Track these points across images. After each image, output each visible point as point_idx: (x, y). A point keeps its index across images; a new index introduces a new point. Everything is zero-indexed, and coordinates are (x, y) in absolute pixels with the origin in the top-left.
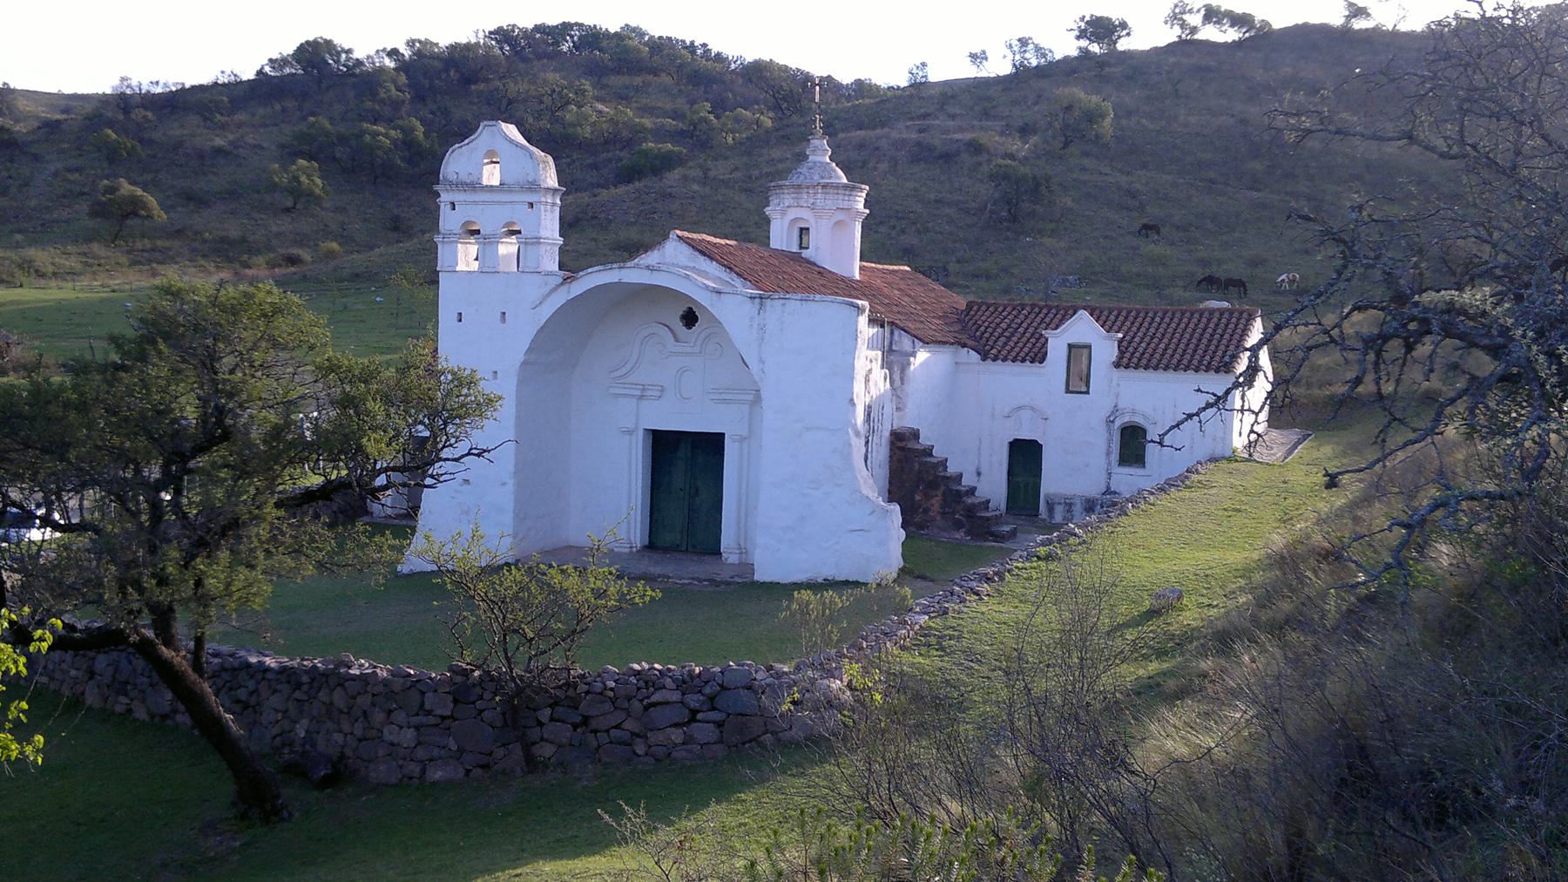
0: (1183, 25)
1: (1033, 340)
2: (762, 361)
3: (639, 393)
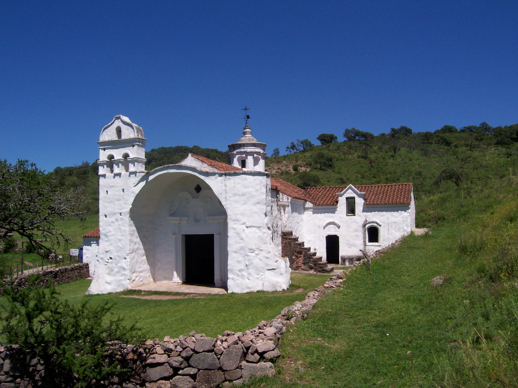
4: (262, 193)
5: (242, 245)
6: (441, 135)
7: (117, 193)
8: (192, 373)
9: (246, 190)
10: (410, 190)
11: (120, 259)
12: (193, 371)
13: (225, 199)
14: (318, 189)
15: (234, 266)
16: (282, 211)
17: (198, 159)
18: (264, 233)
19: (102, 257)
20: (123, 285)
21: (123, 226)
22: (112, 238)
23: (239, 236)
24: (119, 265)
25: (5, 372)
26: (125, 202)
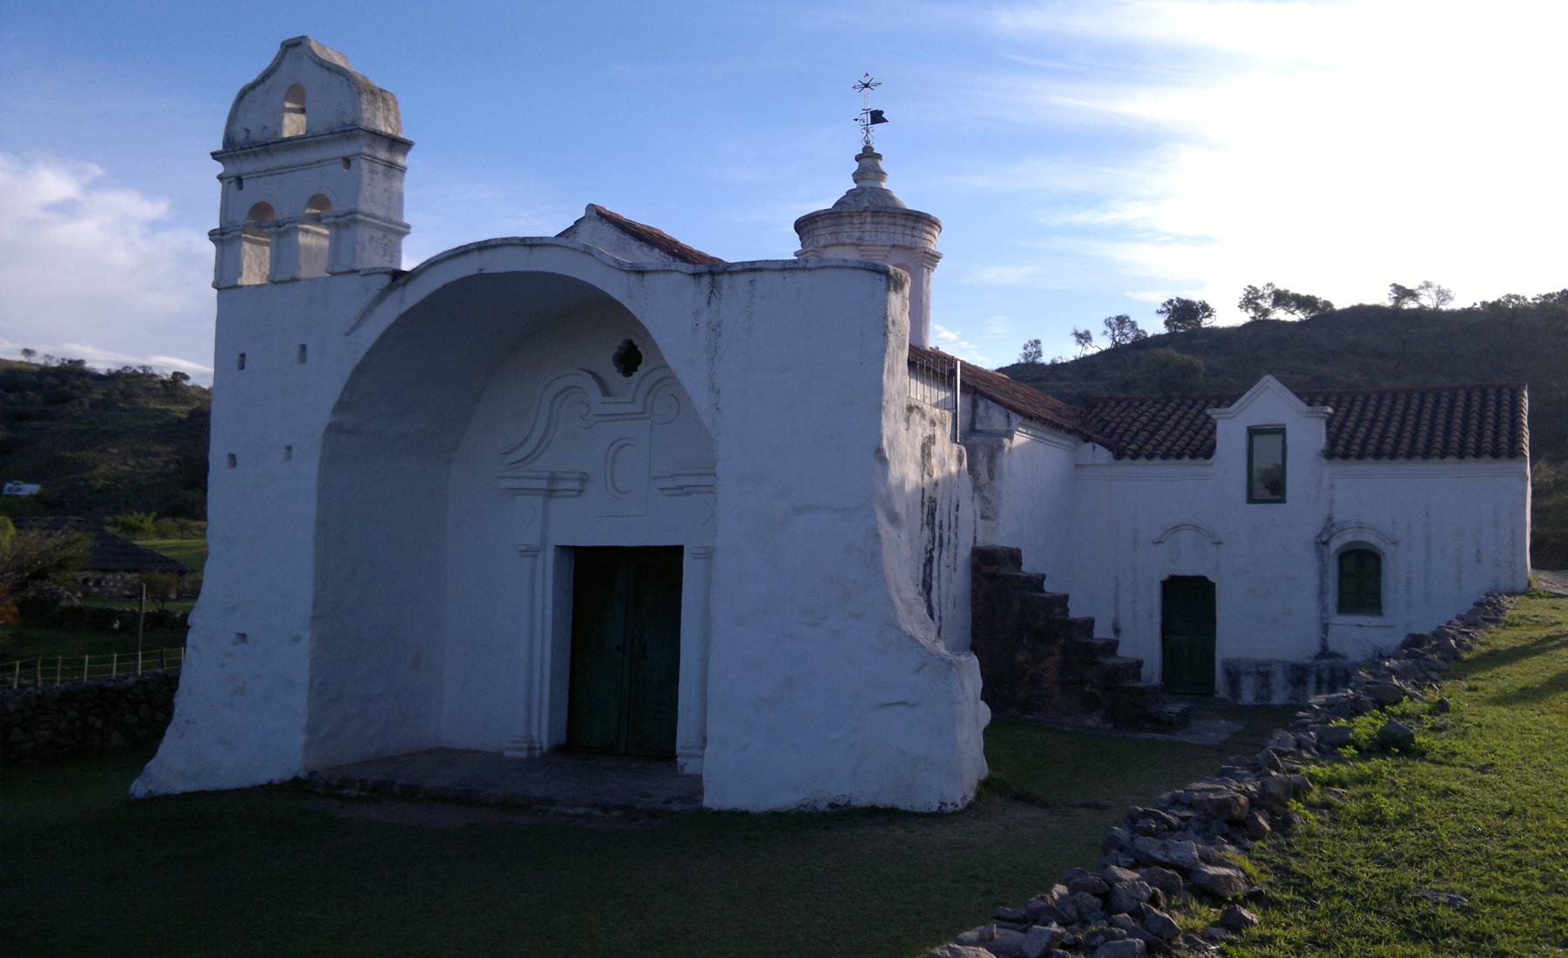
0: (1257, 308)
2: (714, 389)
3: (544, 484)
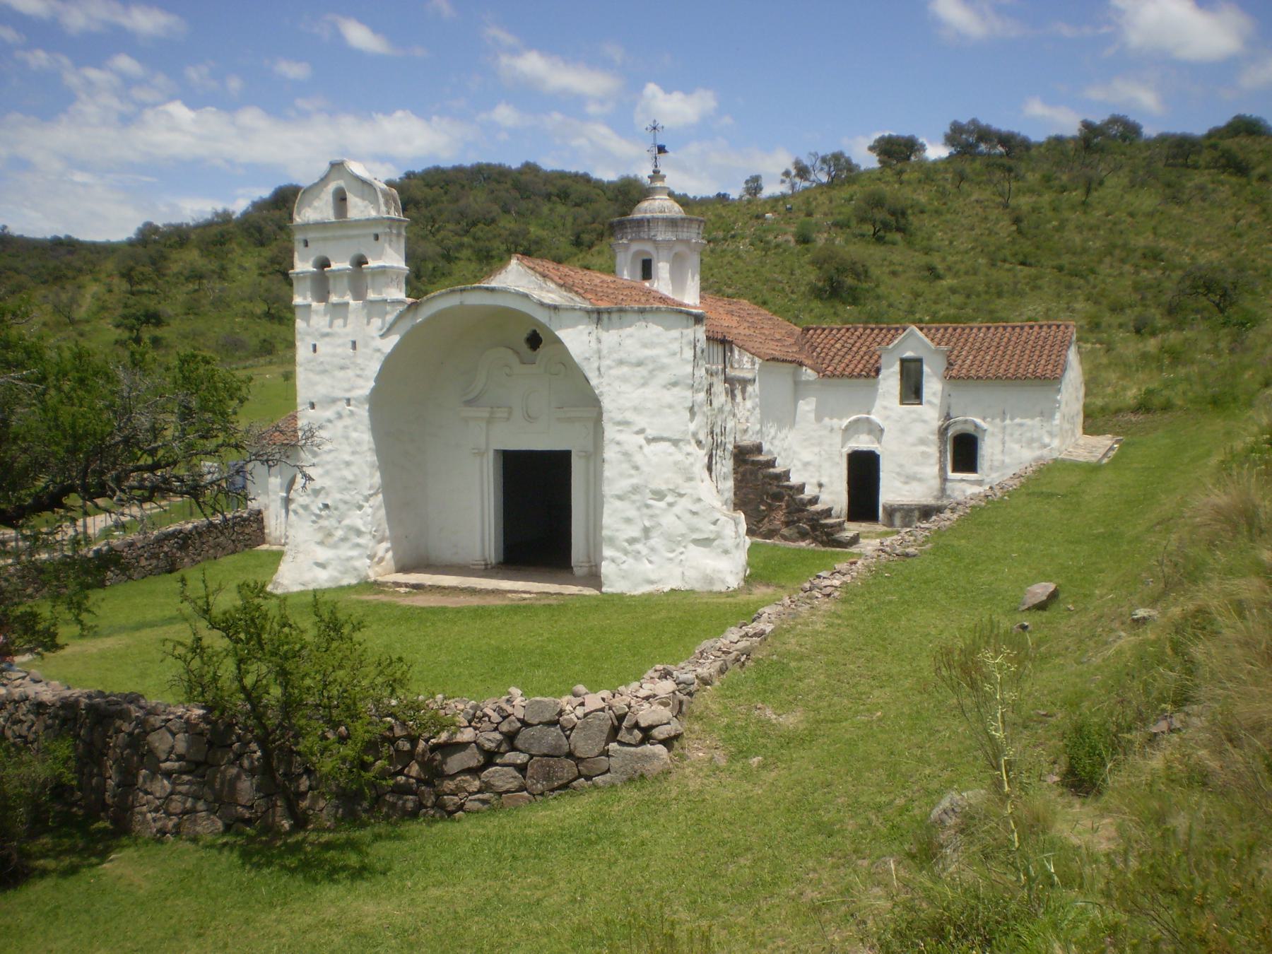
1: (866, 357)
4: (685, 361)
5: (635, 481)
6: (1227, 143)
7: (339, 350)
8: (519, 761)
9: (648, 352)
10: (1066, 343)
11: (349, 510)
12: (521, 758)
13: (597, 373)
14: (834, 332)
15: (617, 530)
16: (738, 393)
17: (533, 269)
18: (688, 454)
19: (304, 503)
20: (355, 569)
21: (355, 430)
22: (328, 458)
23: (630, 461)
24: (346, 522)
25: (177, 755)
26: (359, 372)
